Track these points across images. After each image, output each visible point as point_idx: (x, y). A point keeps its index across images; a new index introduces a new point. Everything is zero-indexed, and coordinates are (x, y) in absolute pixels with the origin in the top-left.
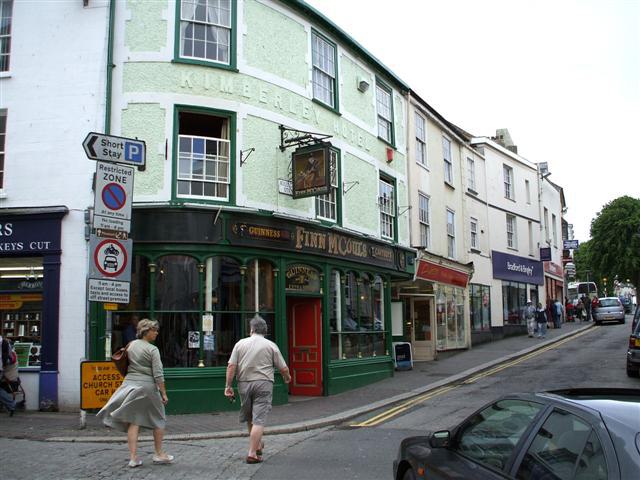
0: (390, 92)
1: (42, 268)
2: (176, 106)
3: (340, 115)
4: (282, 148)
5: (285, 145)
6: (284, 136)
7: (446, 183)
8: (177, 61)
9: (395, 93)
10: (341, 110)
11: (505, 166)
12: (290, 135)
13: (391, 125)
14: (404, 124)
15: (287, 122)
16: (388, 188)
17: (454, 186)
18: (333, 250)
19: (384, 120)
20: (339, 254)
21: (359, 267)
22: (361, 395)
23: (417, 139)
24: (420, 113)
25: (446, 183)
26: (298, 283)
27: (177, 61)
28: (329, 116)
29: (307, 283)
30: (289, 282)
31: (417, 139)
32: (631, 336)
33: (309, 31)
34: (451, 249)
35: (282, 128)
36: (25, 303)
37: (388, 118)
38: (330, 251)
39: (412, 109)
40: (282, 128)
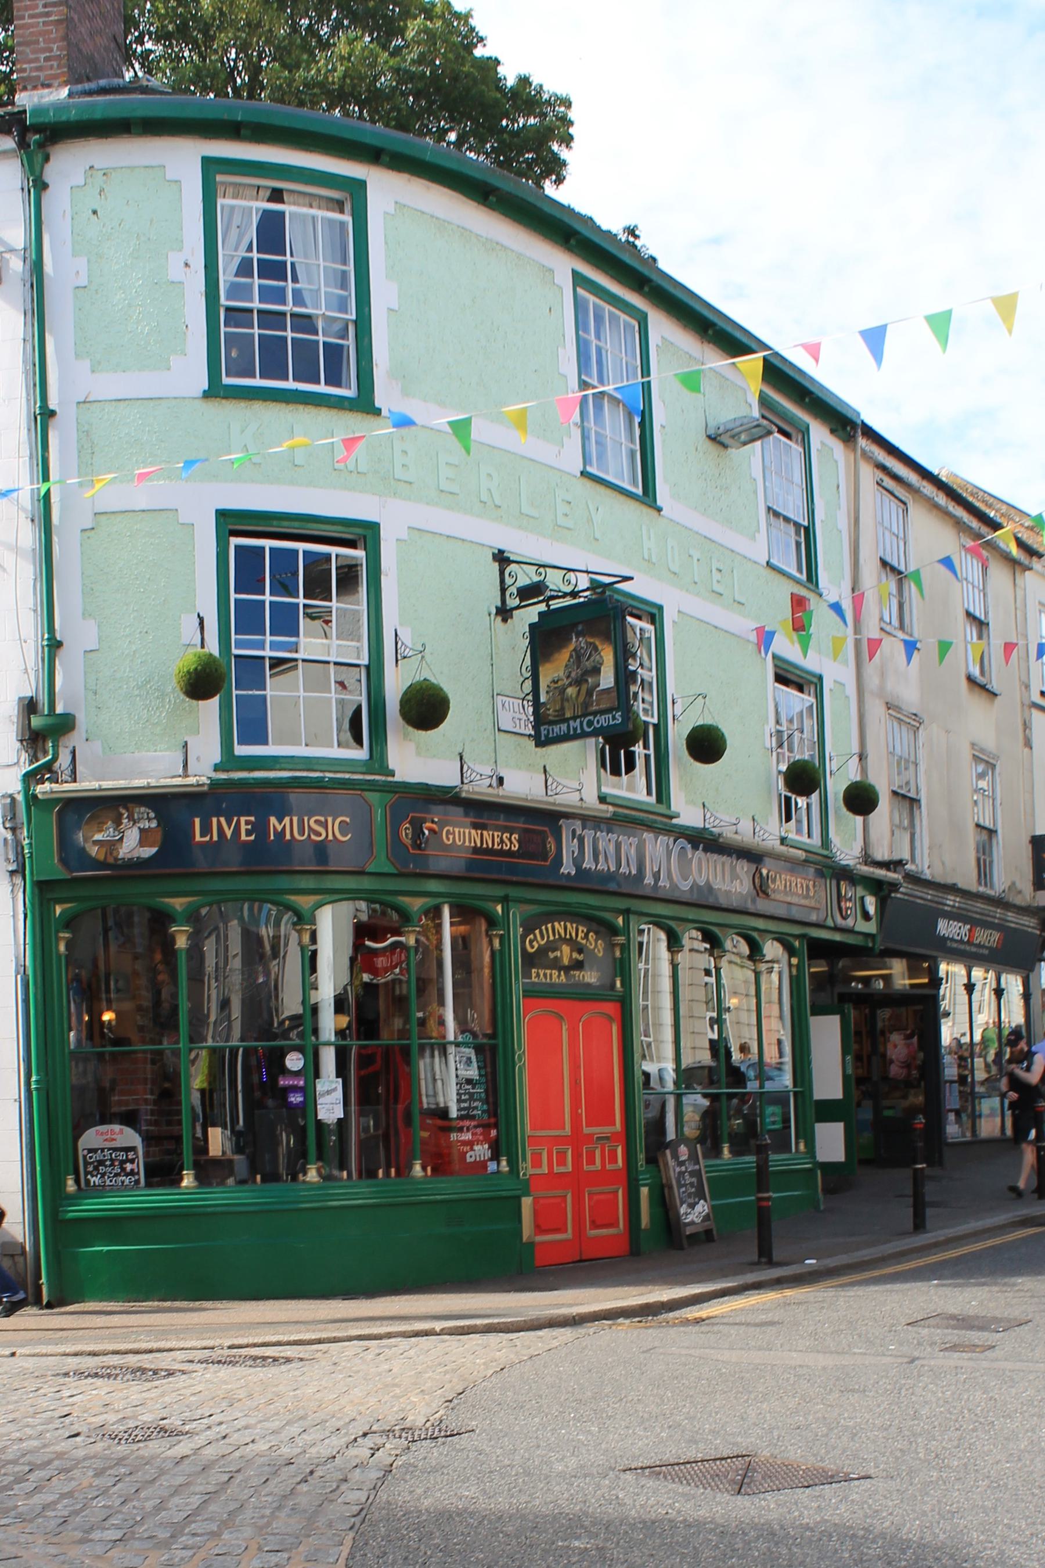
0: (804, 434)
1: (246, 906)
2: (217, 511)
3: (659, 510)
4: (504, 613)
5: (513, 602)
6: (509, 581)
7: (970, 679)
8: (215, 391)
9: (819, 433)
10: (663, 496)
11: (1039, 656)
12: (525, 577)
13: (808, 533)
14: (843, 522)
15: (517, 545)
16: (796, 701)
17: (995, 686)
18: (657, 876)
19: (787, 520)
20: (674, 886)
21: (760, 924)
22: (942, 1536)
23: (884, 563)
24: (889, 483)
25: (970, 679)
26: (556, 964)
27: (215, 391)
28: (634, 512)
29: (579, 965)
30: (530, 961)
31: (884, 563)
32: (29, 778)
33: (567, 282)
34: (984, 870)
35: (502, 559)
36: (615, 814)
37: (797, 513)
38: (649, 880)
39: (868, 475)
40: (502, 559)
